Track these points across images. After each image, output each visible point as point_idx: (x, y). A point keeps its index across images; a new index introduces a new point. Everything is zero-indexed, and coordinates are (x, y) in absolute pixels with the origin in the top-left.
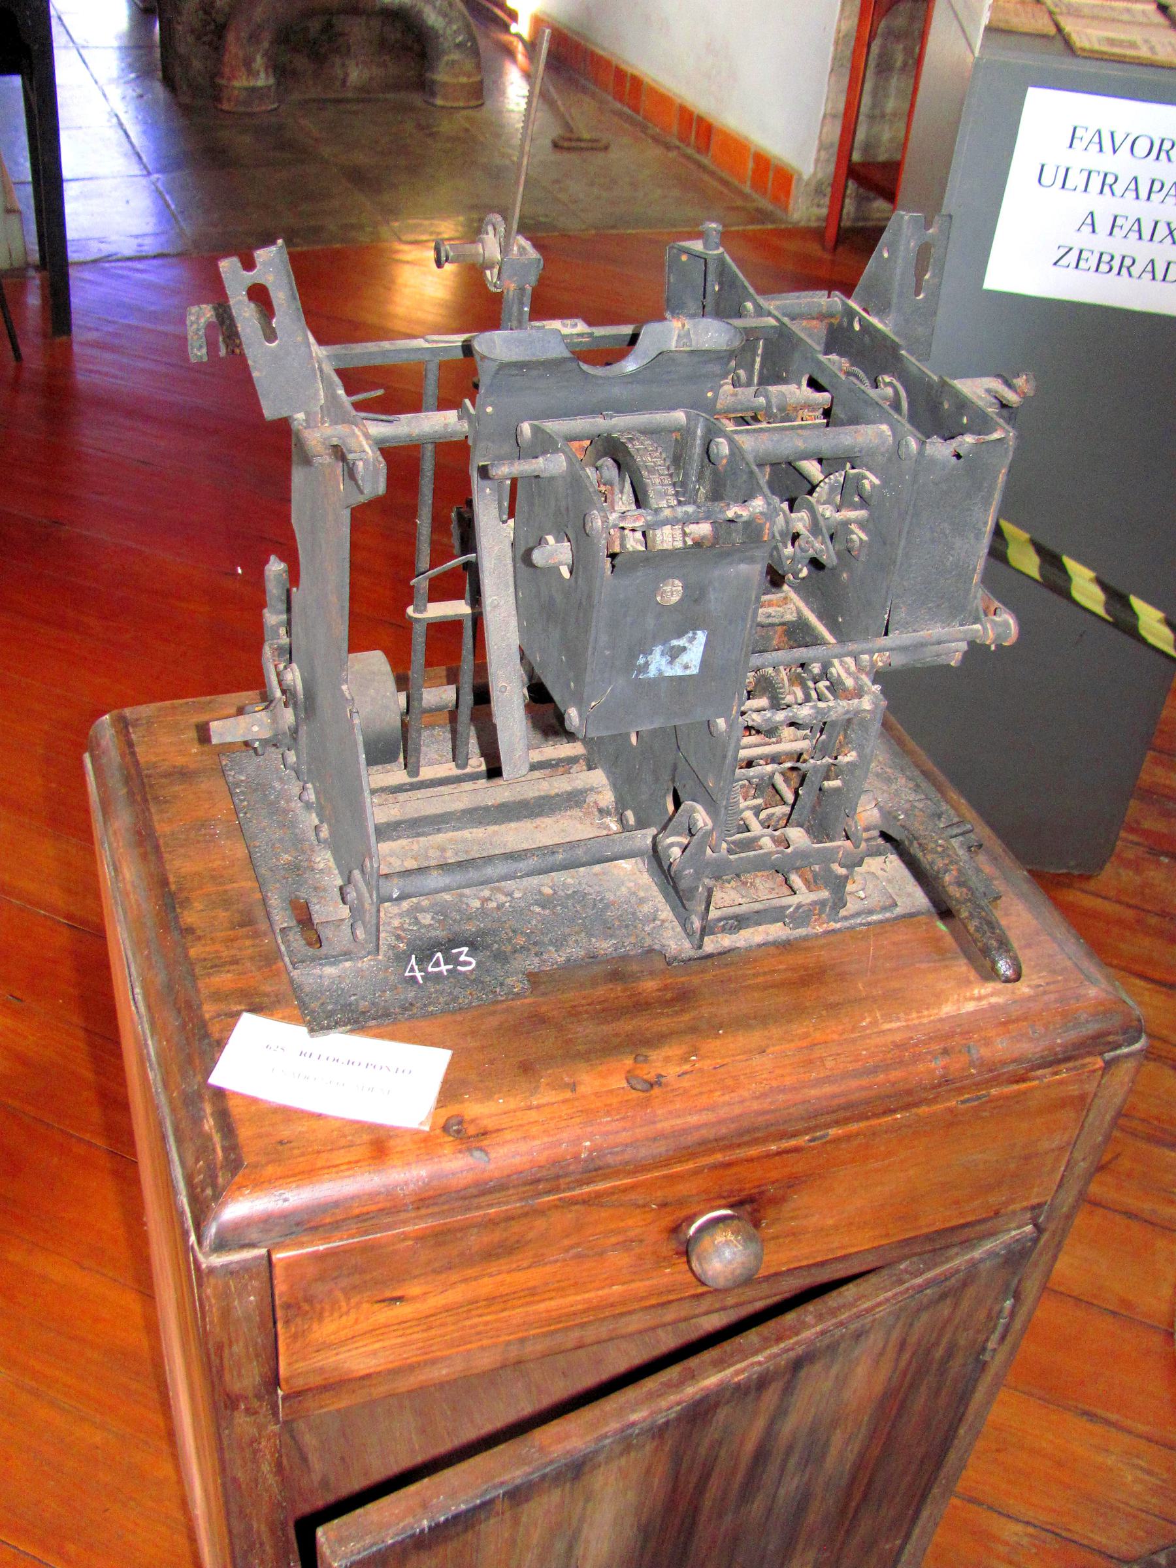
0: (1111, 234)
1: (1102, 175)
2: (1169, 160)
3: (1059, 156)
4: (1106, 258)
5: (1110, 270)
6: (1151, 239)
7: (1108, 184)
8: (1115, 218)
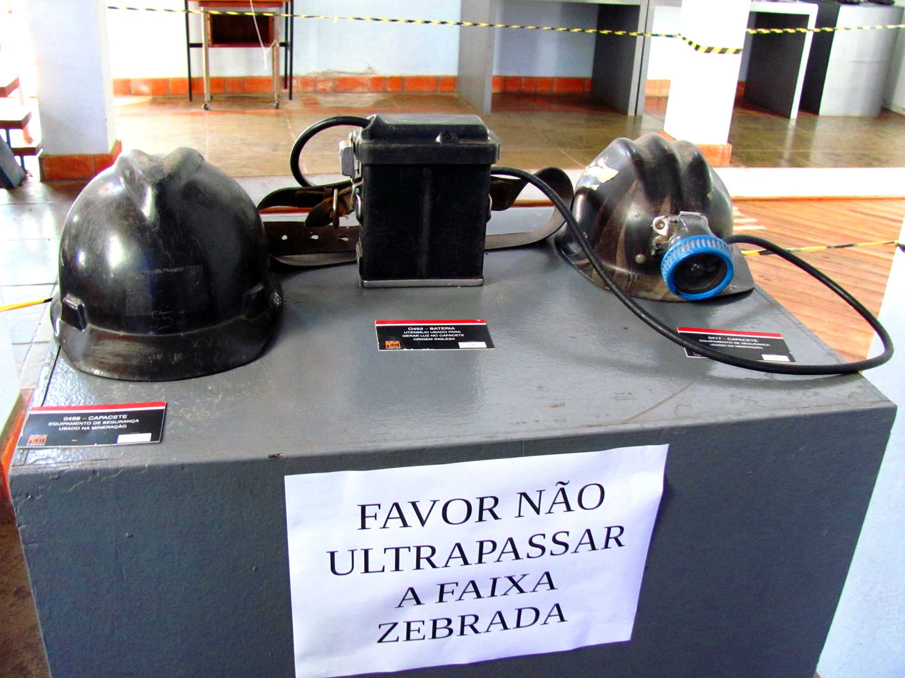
0: (363, 527)
1: (414, 550)
2: (496, 517)
3: (345, 535)
4: (440, 624)
5: (451, 631)
6: (493, 594)
7: (424, 557)
8: (363, 508)
